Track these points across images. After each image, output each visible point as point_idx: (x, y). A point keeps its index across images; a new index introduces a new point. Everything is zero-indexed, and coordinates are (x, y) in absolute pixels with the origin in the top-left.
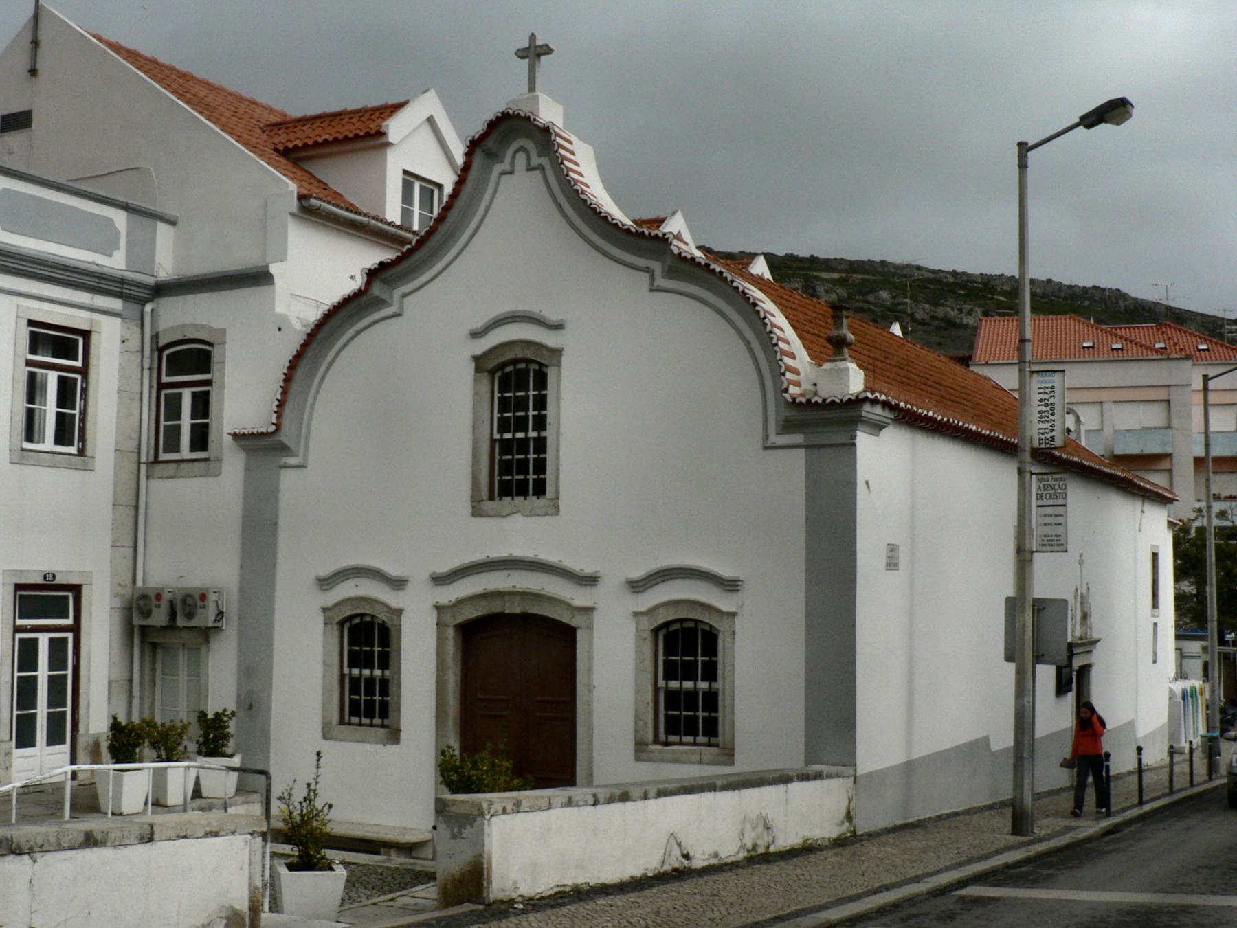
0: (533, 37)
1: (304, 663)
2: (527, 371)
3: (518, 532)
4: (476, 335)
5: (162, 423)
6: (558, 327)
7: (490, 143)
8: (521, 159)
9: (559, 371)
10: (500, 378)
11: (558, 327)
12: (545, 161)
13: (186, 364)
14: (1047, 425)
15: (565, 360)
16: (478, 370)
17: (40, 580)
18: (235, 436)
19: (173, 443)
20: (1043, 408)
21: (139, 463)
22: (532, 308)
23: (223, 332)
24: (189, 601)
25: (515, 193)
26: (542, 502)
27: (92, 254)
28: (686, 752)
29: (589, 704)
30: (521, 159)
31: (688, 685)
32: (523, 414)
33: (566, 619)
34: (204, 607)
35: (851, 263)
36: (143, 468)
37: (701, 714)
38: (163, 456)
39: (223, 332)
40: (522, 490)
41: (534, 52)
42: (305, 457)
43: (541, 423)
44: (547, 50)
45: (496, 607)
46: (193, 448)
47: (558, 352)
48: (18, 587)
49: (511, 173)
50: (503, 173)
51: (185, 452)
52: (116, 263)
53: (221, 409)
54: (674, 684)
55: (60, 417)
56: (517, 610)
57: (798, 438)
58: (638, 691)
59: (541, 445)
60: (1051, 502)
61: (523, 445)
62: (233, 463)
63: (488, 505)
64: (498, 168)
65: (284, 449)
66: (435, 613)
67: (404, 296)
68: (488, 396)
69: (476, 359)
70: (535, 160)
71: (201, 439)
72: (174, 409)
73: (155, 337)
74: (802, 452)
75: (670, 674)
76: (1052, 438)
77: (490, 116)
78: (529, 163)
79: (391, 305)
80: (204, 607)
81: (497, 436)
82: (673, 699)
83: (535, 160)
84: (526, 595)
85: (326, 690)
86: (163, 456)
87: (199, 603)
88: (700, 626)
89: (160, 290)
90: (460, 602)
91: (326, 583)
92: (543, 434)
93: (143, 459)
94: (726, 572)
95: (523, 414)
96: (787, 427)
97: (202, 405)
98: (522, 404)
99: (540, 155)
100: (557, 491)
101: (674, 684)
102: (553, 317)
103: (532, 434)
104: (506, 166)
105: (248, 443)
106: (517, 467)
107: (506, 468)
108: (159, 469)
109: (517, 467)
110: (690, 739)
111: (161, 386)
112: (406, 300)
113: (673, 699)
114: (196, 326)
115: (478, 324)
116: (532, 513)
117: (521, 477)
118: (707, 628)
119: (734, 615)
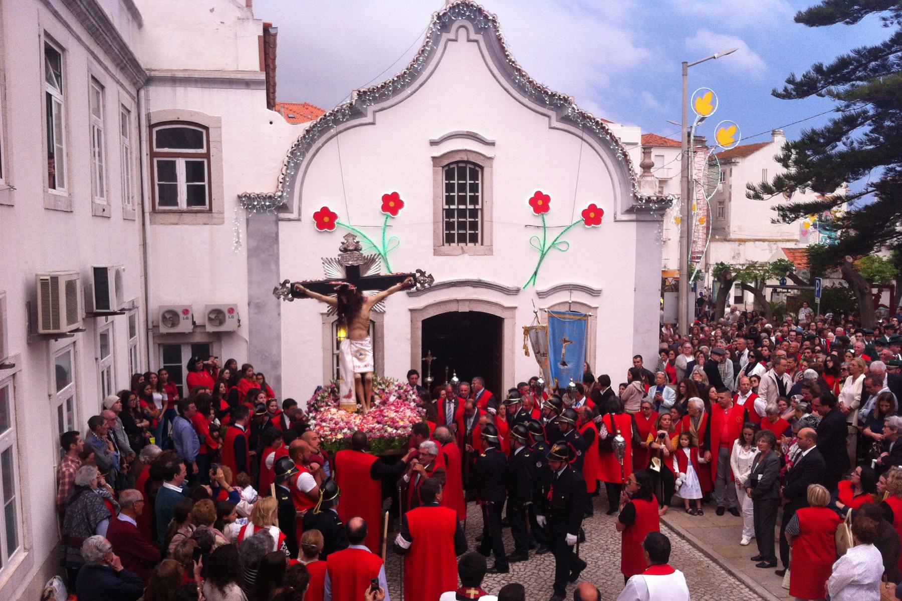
2: (465, 168)
8: (462, 32)
11: (493, 144)
12: (479, 37)
15: (495, 163)
19: (168, 196)
23: (219, 120)
33: (498, 313)
35: (135, 60)
36: (147, 216)
38: (294, 216)
42: (300, 214)
43: (474, 200)
45: (452, 308)
46: (190, 203)
49: (456, 40)
55: (61, 144)
57: (633, 217)
59: (449, 200)
62: (232, 217)
66: (409, 313)
70: (473, 36)
71: (197, 196)
72: (167, 171)
73: (148, 115)
74: (635, 223)
78: (468, 37)
79: (366, 116)
83: (473, 36)
90: (426, 307)
97: (196, 171)
100: (492, 241)
102: (489, 138)
104: (452, 35)
106: (462, 222)
109: (462, 222)
111: (153, 155)
116: (475, 254)
119: (596, 308)
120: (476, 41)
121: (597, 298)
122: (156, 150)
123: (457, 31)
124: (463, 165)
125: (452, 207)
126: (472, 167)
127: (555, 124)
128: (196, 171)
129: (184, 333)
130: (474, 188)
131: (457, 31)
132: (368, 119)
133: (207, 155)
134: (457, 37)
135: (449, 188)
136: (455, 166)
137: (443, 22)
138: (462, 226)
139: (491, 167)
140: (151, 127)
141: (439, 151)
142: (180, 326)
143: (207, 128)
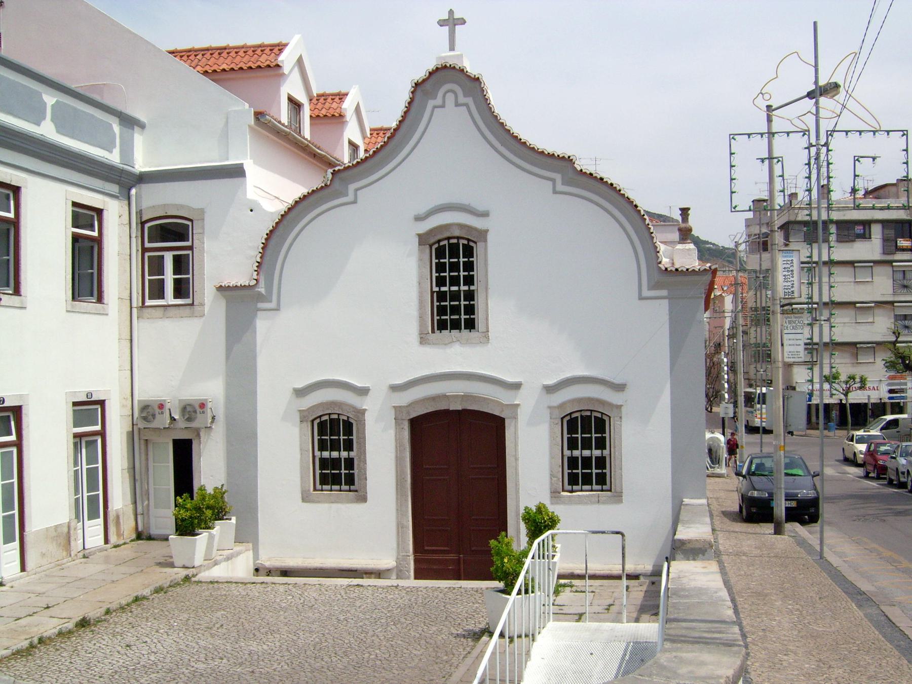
0: (451, 12)
1: (284, 452)
2: (458, 244)
3: (456, 355)
4: (419, 219)
5: (147, 277)
6: (485, 215)
7: (428, 85)
9: (486, 246)
10: (436, 249)
12: (470, 101)
13: (169, 236)
14: (789, 284)
15: (490, 237)
16: (421, 243)
17: (85, 399)
18: (220, 288)
19: (157, 291)
20: (786, 273)
21: (131, 308)
22: (464, 200)
23: (202, 211)
24: (189, 409)
25: (448, 118)
26: (473, 334)
27: (102, 151)
28: (587, 496)
29: (516, 469)
30: (450, 98)
31: (335, 454)
32: (456, 274)
34: (203, 412)
36: (135, 311)
37: (594, 471)
38: (149, 303)
39: (202, 211)
40: (456, 325)
41: (452, 22)
43: (469, 280)
44: (463, 22)
47: (483, 234)
48: (75, 404)
49: (443, 106)
50: (435, 107)
51: (169, 297)
52: (114, 157)
53: (202, 267)
54: (326, 454)
56: (460, 408)
57: (664, 293)
58: (552, 457)
59: (470, 296)
60: (793, 331)
61: (455, 296)
63: (432, 337)
64: (431, 103)
65: (261, 298)
67: (357, 190)
68: (428, 264)
69: (420, 236)
71: (181, 289)
72: (157, 266)
73: (140, 213)
75: (322, 448)
76: (793, 292)
77: (431, 66)
80: (203, 412)
81: (436, 289)
82: (324, 463)
83: (462, 99)
84: (434, 399)
85: (303, 469)
86: (149, 303)
87: (198, 410)
88: (342, 417)
89: (143, 178)
91: (300, 393)
92: (472, 288)
93: (135, 304)
94: (510, 379)
95: (456, 274)
96: (654, 286)
97: (181, 264)
98: (454, 267)
99: (465, 96)
101: (326, 454)
102: (481, 208)
103: (464, 288)
104: (438, 101)
105: (228, 293)
107: (442, 311)
108: (146, 311)
109: (454, 305)
110: (337, 487)
111: (144, 250)
112: (359, 192)
113: (324, 463)
114: (182, 207)
115: (422, 210)
116: (468, 342)
117: (443, 317)
118: (599, 415)
120: (467, 105)
121: (620, 394)
122: (147, 245)
123: (444, 96)
124: (455, 241)
125: (443, 289)
126: (465, 242)
127: (560, 187)
128: (181, 264)
129: (159, 429)
130: (469, 266)
131: (444, 96)
132: (350, 197)
133: (191, 248)
134: (444, 102)
135: (440, 268)
136: (446, 242)
137: (422, 89)
138: (455, 310)
139: (485, 241)
140: (143, 224)
141: (425, 227)
142: (196, 421)
143: (191, 221)
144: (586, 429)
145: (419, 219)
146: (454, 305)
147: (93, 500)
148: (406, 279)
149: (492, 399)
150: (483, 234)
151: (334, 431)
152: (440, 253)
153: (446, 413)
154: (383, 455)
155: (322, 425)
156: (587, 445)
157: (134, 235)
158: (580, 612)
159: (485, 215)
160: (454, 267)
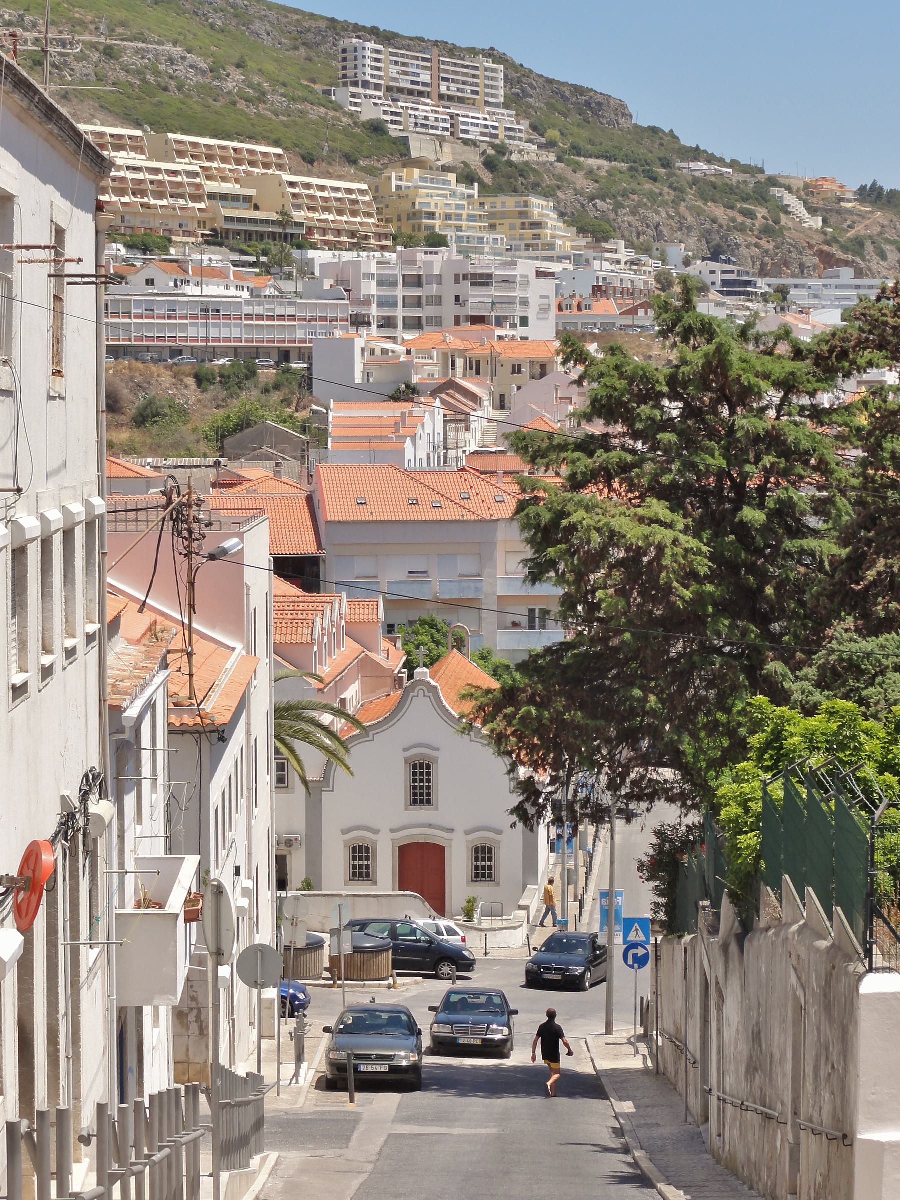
3: (421, 814)
4: (405, 750)
6: (438, 750)
43: (429, 781)
59: (429, 788)
98: (422, 774)
104: (415, 694)
109: (421, 791)
130: (429, 774)
144: (483, 852)
145: (405, 750)
146: (421, 791)
147: (227, 219)
148: (399, 782)
149: (436, 837)
150: (436, 760)
151: (361, 851)
152: (415, 767)
153: (417, 844)
154: (385, 865)
155: (354, 849)
156: (483, 860)
157: (18, 321)
158: (147, 626)
159: (438, 750)
160: (422, 774)
